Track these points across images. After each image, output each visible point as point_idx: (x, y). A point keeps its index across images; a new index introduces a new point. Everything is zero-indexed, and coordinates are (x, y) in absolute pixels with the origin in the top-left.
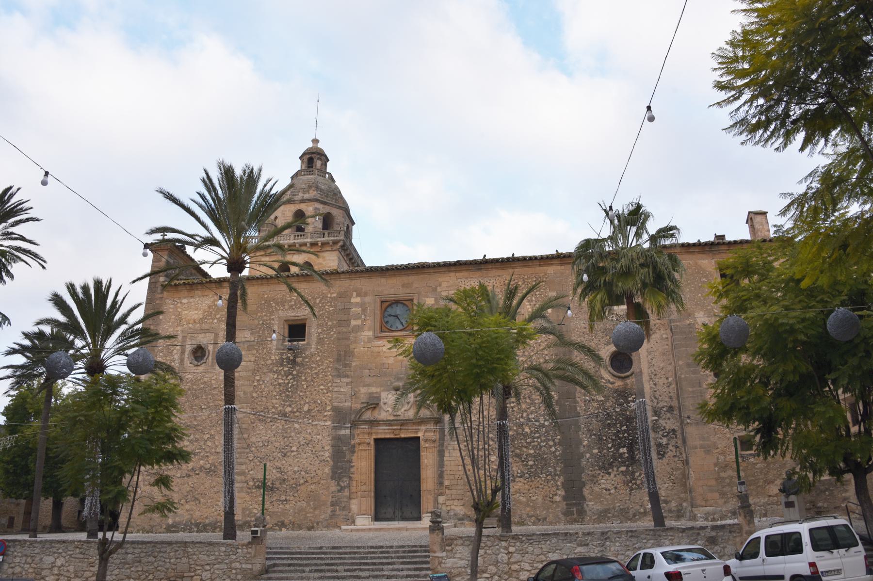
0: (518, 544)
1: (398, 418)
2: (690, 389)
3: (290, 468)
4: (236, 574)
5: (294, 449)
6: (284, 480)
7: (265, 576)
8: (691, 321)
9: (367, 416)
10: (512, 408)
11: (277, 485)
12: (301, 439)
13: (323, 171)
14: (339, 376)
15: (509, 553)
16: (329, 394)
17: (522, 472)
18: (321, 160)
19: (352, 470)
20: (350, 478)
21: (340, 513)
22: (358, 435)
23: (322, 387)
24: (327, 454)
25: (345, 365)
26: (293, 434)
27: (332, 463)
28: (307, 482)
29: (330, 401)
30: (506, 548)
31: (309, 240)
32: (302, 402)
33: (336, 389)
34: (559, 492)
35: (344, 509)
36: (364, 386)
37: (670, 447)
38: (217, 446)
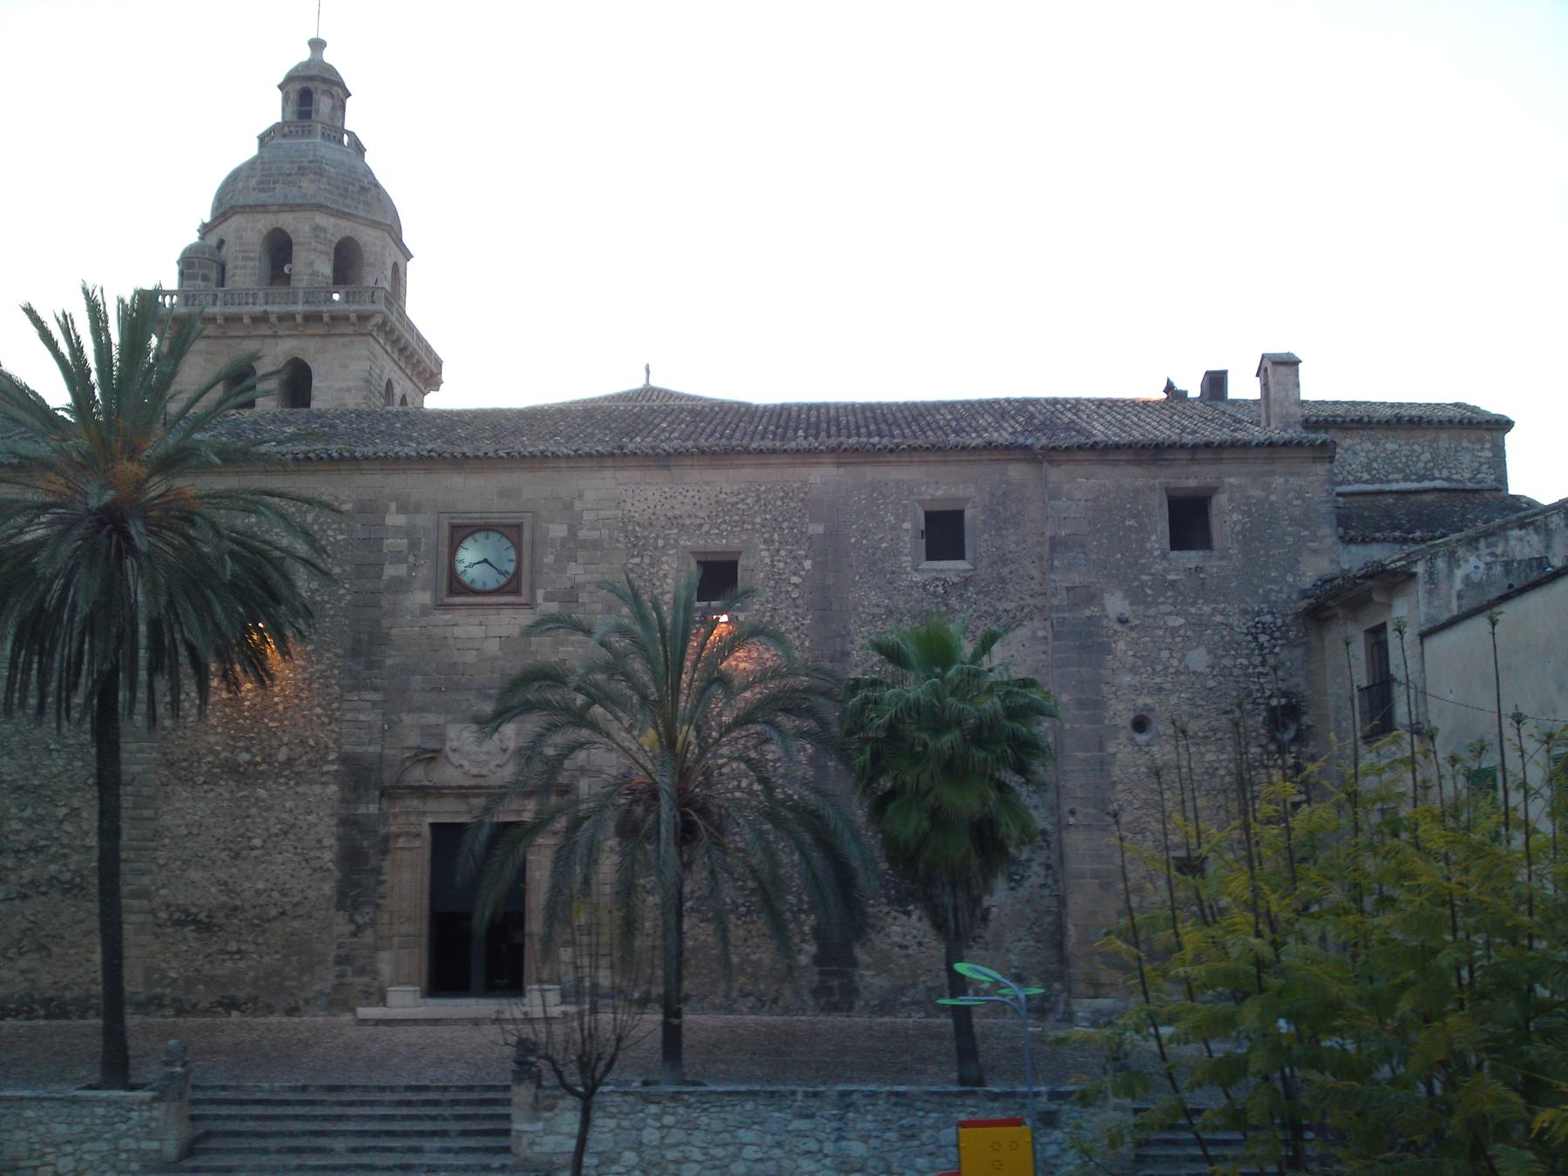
0: (681, 1110)
1: (482, 782)
2: (1080, 755)
3: (247, 885)
4: (129, 1161)
5: (257, 842)
6: (235, 909)
7: (188, 1163)
8: (1094, 610)
9: (417, 775)
10: (720, 767)
11: (220, 917)
12: (272, 821)
13: (336, 131)
14: (356, 688)
15: (664, 1126)
16: (333, 726)
17: (733, 902)
18: (332, 96)
19: (382, 889)
20: (378, 906)
21: (354, 983)
22: (396, 816)
23: (318, 710)
24: (328, 855)
25: (371, 665)
26: (253, 811)
27: (337, 874)
28: (283, 913)
29: (336, 741)
30: (658, 1117)
31: (300, 308)
32: (275, 742)
33: (349, 716)
34: (806, 947)
35: (362, 971)
36: (411, 711)
37: (1035, 867)
38: (86, 833)
